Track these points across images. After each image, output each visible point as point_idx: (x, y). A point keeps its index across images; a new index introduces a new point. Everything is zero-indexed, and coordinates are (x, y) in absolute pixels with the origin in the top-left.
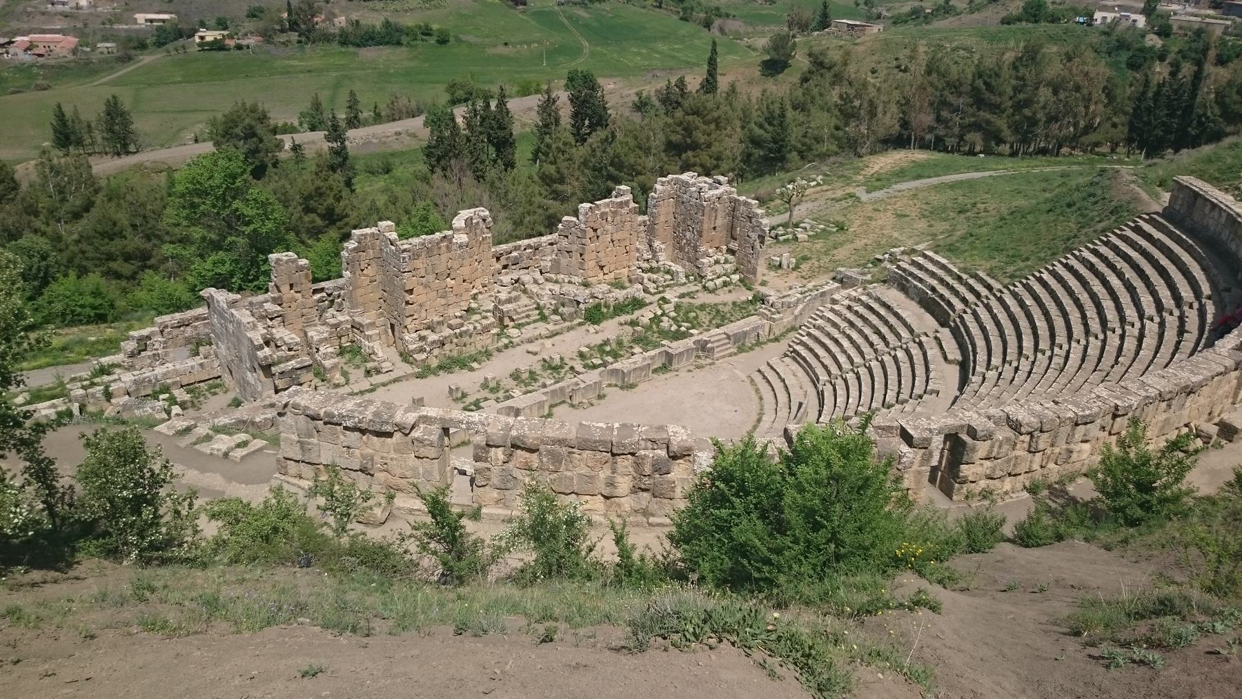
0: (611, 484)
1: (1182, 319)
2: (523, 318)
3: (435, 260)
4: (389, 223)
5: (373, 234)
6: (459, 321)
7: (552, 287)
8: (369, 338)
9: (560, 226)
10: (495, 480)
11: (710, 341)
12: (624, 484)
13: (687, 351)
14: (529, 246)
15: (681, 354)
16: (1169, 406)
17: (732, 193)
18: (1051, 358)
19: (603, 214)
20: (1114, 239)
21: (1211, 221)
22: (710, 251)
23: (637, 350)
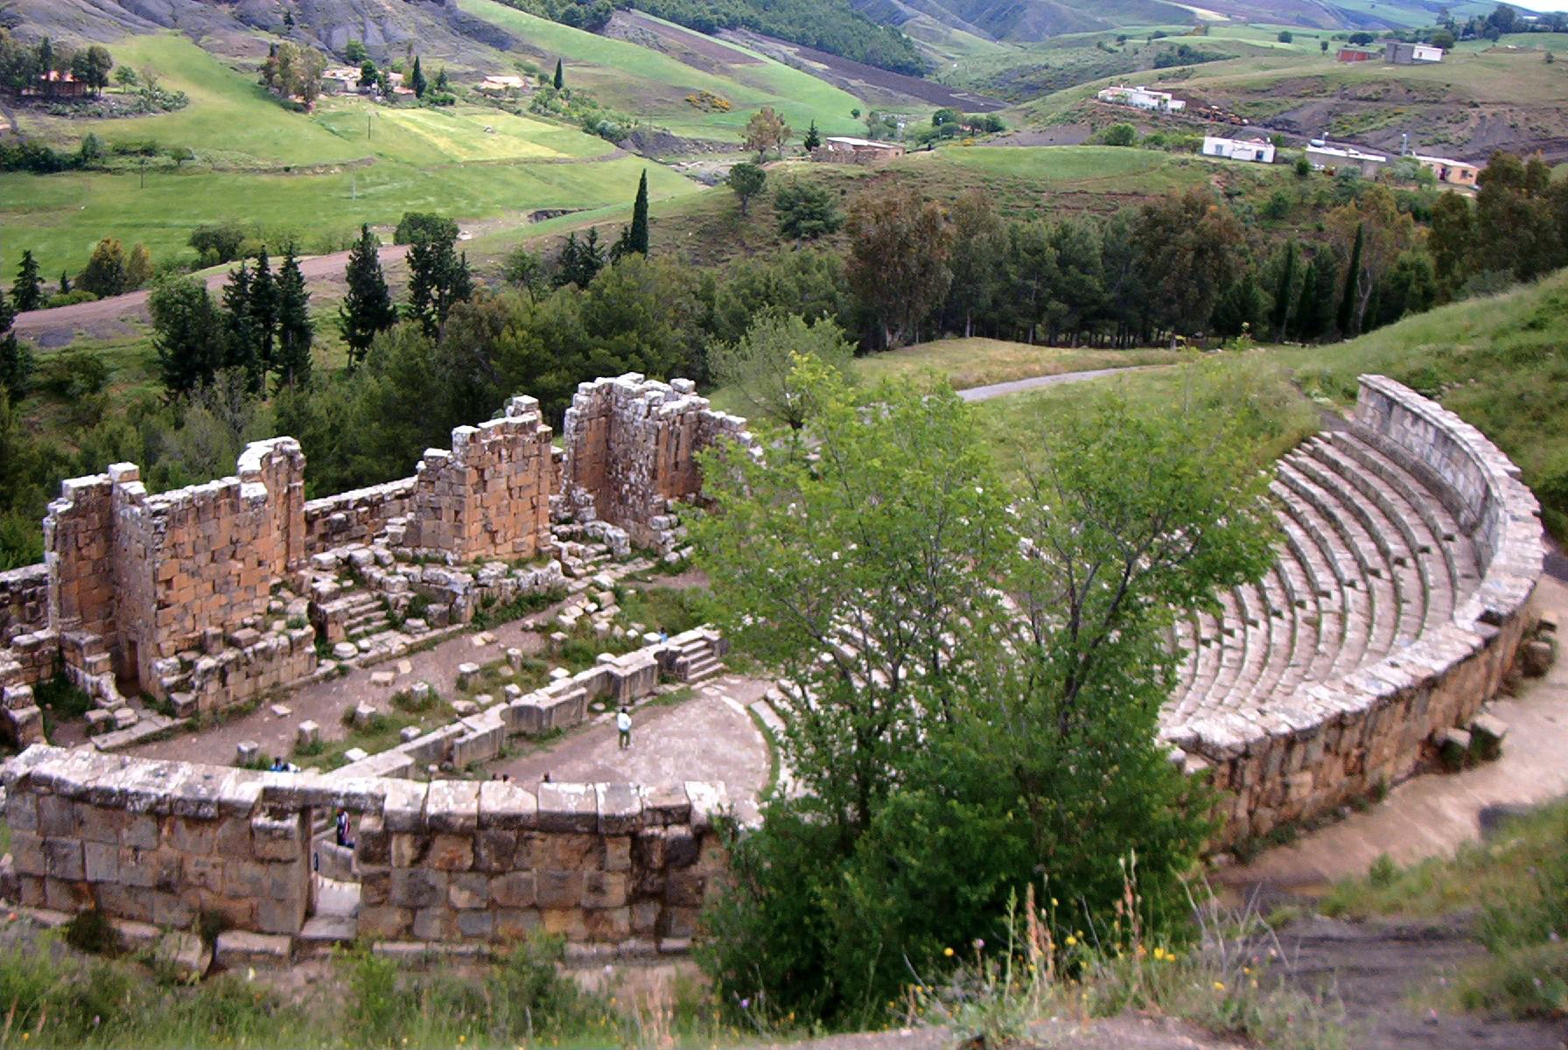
0: (597, 889)
1: (1395, 582)
2: (359, 624)
3: (211, 527)
4: (129, 466)
5: (100, 485)
6: (250, 632)
7: (408, 570)
8: (89, 667)
9: (421, 465)
10: (398, 893)
11: (680, 653)
12: (617, 887)
13: (645, 669)
14: (362, 502)
15: (634, 675)
16: (1408, 708)
17: (702, 406)
18: (1220, 655)
19: (493, 445)
20: (1285, 467)
21: (1415, 440)
22: (670, 502)
23: (560, 673)
